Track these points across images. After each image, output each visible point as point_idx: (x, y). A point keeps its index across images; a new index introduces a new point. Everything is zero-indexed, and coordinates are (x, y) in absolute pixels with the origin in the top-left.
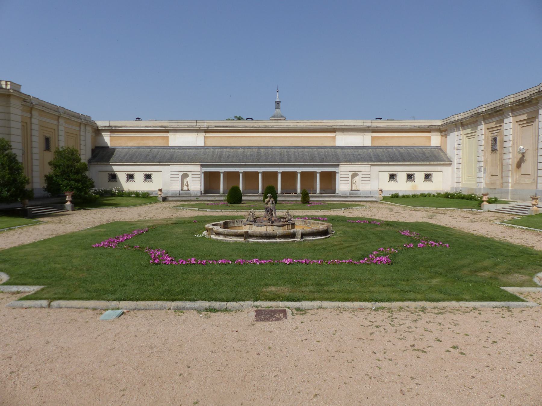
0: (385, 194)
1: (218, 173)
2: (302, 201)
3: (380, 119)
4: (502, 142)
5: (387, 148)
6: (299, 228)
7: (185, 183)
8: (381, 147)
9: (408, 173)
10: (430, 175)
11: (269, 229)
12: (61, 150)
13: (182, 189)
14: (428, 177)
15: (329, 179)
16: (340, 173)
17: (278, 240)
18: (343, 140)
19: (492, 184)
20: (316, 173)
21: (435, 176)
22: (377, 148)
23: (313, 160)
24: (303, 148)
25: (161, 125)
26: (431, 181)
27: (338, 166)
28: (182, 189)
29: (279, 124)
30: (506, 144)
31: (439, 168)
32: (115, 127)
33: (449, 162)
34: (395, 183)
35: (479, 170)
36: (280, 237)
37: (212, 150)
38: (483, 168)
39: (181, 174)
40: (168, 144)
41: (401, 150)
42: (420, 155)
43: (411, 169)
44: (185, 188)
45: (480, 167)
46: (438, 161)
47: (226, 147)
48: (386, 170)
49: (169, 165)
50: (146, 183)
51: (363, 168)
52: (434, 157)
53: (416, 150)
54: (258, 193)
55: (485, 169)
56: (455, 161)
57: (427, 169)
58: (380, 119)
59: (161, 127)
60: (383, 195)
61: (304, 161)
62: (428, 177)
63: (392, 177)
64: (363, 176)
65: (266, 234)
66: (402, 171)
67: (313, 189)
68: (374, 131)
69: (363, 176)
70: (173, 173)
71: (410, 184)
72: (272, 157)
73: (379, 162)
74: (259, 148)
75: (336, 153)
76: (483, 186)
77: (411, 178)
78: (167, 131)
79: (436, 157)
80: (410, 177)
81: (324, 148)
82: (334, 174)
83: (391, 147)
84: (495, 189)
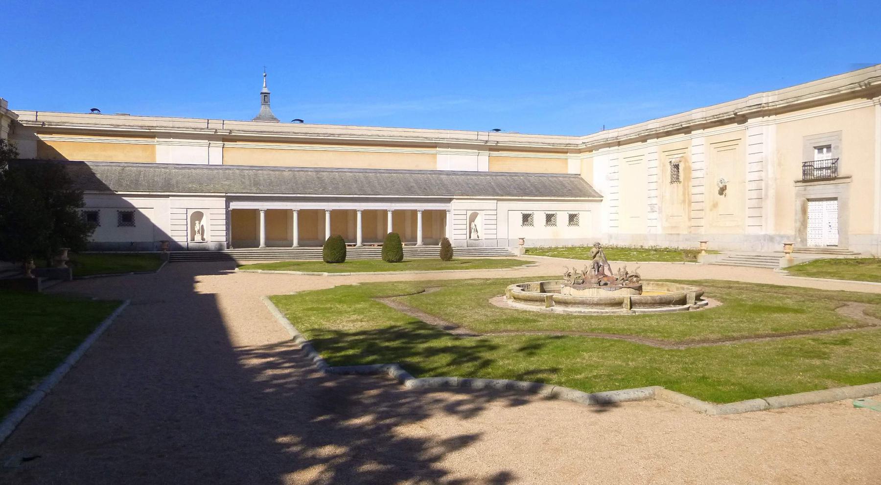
1: (255, 213)
2: (441, 255)
3: (302, 121)
4: (688, 169)
5: (511, 174)
6: (650, 292)
7: (197, 228)
8: (503, 174)
11: (604, 294)
13: (193, 239)
15: (435, 220)
16: (453, 212)
17: (673, 308)
18: (449, 162)
20: (323, 211)
21: (582, 218)
22: (497, 174)
23: (410, 190)
24: (389, 171)
25: (140, 123)
26: (120, 225)
27: (449, 200)
28: (193, 239)
29: (350, 132)
30: (695, 174)
32: (50, 123)
33: (596, 197)
34: (531, 227)
36: (597, 304)
37: (237, 171)
38: (657, 206)
39: (190, 212)
40: (154, 158)
41: (532, 179)
42: (559, 187)
44: (198, 238)
45: (652, 206)
46: (585, 196)
47: (262, 168)
49: (168, 196)
50: (525, 227)
51: (484, 205)
52: (572, 189)
54: (291, 245)
56: (607, 198)
57: (571, 207)
58: (302, 121)
59: (141, 127)
60: (525, 246)
61: (398, 193)
62: (572, 218)
63: (526, 218)
64: (487, 217)
65: (661, 299)
66: (539, 208)
67: (286, 239)
68: (492, 149)
69: (487, 217)
70: (175, 211)
72: (344, 185)
74: (318, 171)
75: (441, 180)
76: (659, 231)
78: (152, 135)
79: (581, 191)
81: (421, 172)
82: (442, 214)
83: (516, 174)
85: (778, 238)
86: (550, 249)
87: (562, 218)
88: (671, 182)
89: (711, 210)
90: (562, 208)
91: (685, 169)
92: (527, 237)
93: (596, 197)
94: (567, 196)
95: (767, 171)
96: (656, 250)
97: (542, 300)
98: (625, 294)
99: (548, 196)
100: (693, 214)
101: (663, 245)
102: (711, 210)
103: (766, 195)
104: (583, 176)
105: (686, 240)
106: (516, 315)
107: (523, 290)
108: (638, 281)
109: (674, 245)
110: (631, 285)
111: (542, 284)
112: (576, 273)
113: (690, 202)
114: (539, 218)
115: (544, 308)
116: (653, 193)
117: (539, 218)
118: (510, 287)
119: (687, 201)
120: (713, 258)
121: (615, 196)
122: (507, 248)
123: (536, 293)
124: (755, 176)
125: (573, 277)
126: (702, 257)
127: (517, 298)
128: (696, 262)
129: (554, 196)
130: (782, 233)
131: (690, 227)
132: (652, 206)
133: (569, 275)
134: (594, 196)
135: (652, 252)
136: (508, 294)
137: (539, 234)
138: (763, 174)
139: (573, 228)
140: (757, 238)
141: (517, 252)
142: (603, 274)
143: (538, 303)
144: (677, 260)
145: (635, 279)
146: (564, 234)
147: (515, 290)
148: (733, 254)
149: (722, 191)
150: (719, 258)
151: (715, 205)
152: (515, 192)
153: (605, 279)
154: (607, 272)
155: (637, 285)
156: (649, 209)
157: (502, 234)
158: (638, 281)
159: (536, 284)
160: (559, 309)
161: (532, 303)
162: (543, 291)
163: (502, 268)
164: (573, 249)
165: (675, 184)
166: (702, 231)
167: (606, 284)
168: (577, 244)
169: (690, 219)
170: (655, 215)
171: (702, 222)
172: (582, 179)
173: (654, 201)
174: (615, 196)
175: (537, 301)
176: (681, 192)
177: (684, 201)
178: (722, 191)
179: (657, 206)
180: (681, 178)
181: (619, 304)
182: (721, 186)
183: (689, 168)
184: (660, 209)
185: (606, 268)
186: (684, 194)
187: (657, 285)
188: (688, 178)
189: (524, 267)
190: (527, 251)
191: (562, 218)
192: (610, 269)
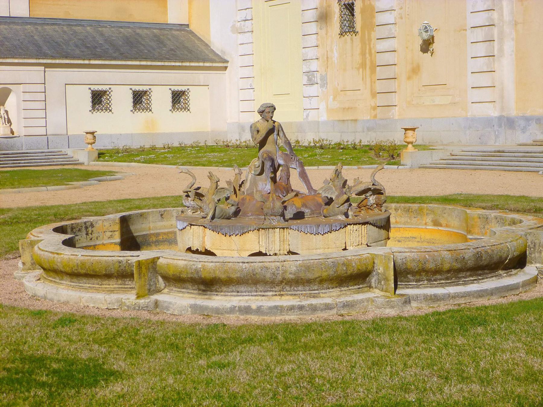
0: (101, 145)
9: (173, 88)
10: (183, 93)
12: (112, 378)
14: (178, 98)
19: (345, 110)
21: (196, 97)
31: (201, 76)
33: (216, 62)
35: (309, 79)
38: (318, 75)
43: (141, 78)
45: (309, 74)
46: (198, 60)
48: (74, 83)
53: (138, 31)
55: (324, 79)
56: (236, 62)
57: (177, 78)
62: (178, 98)
63: (98, 99)
64: (28, 97)
66: (120, 81)
69: (28, 97)
71: (141, 116)
73: (66, 57)
77: (100, 102)
79: (190, 52)
80: (139, 98)
83: (79, 22)
84: (356, 120)
85: (522, 123)
86: (142, 151)
87: (160, 98)
88: (341, 34)
89: (409, 78)
90: (160, 82)
91: (363, 11)
92: (99, 132)
93: (216, 62)
94: (169, 59)
95: (501, 9)
96: (321, 147)
97: (123, 275)
98: (350, 244)
99: (136, 59)
100: (379, 86)
101: (333, 137)
102: (409, 78)
103: (501, 50)
104: (192, 28)
105: (369, 129)
106: (34, 345)
107: (66, 243)
108: (379, 205)
109: (349, 138)
110: (364, 215)
111: (124, 221)
112: (217, 189)
113: (374, 67)
114: (121, 98)
115: (130, 298)
116: (311, 53)
117: (121, 98)
118: (35, 234)
119: (369, 64)
120: (425, 158)
121: (247, 60)
122: (65, 150)
123: (111, 254)
124: (481, 19)
125: (210, 199)
126: (409, 156)
127: (53, 271)
128: (398, 164)
129: (146, 59)
130: (529, 113)
131: (374, 108)
132: (309, 74)
133: (199, 196)
134: (212, 61)
135: (318, 151)
136: (26, 257)
137: (121, 124)
138: (495, 15)
139: (180, 115)
140: (488, 122)
141: (83, 157)
142: (288, 189)
143: (113, 284)
144: (365, 163)
145: (372, 199)
146: (164, 124)
147: (47, 241)
148: (457, 150)
149: (427, 45)
150: (436, 157)
151: (416, 70)
152: (77, 52)
153: (298, 202)
154: (296, 183)
155: (377, 215)
156: (305, 80)
157: (56, 122)
158: (379, 205)
159: (108, 227)
160: (179, 303)
161: (95, 283)
162: (130, 242)
163: (46, 184)
164: (182, 149)
165: (348, 37)
166: (395, 113)
167: (299, 216)
168: (188, 142)
169: (374, 94)
170: (314, 90)
171: (395, 99)
172: (192, 33)
173: (314, 66)
174: (247, 60)
175: (108, 276)
176: (358, 51)
177: (363, 65)
178: (427, 45)
179: (318, 75)
180: (358, 26)
181: (360, 277)
182: (425, 36)
183: (372, 8)
184: (324, 79)
185: (294, 174)
186: (363, 54)
187: (408, 210)
188: (370, 26)
189: (92, 181)
190: (101, 155)
191: (160, 98)
192: (303, 175)
